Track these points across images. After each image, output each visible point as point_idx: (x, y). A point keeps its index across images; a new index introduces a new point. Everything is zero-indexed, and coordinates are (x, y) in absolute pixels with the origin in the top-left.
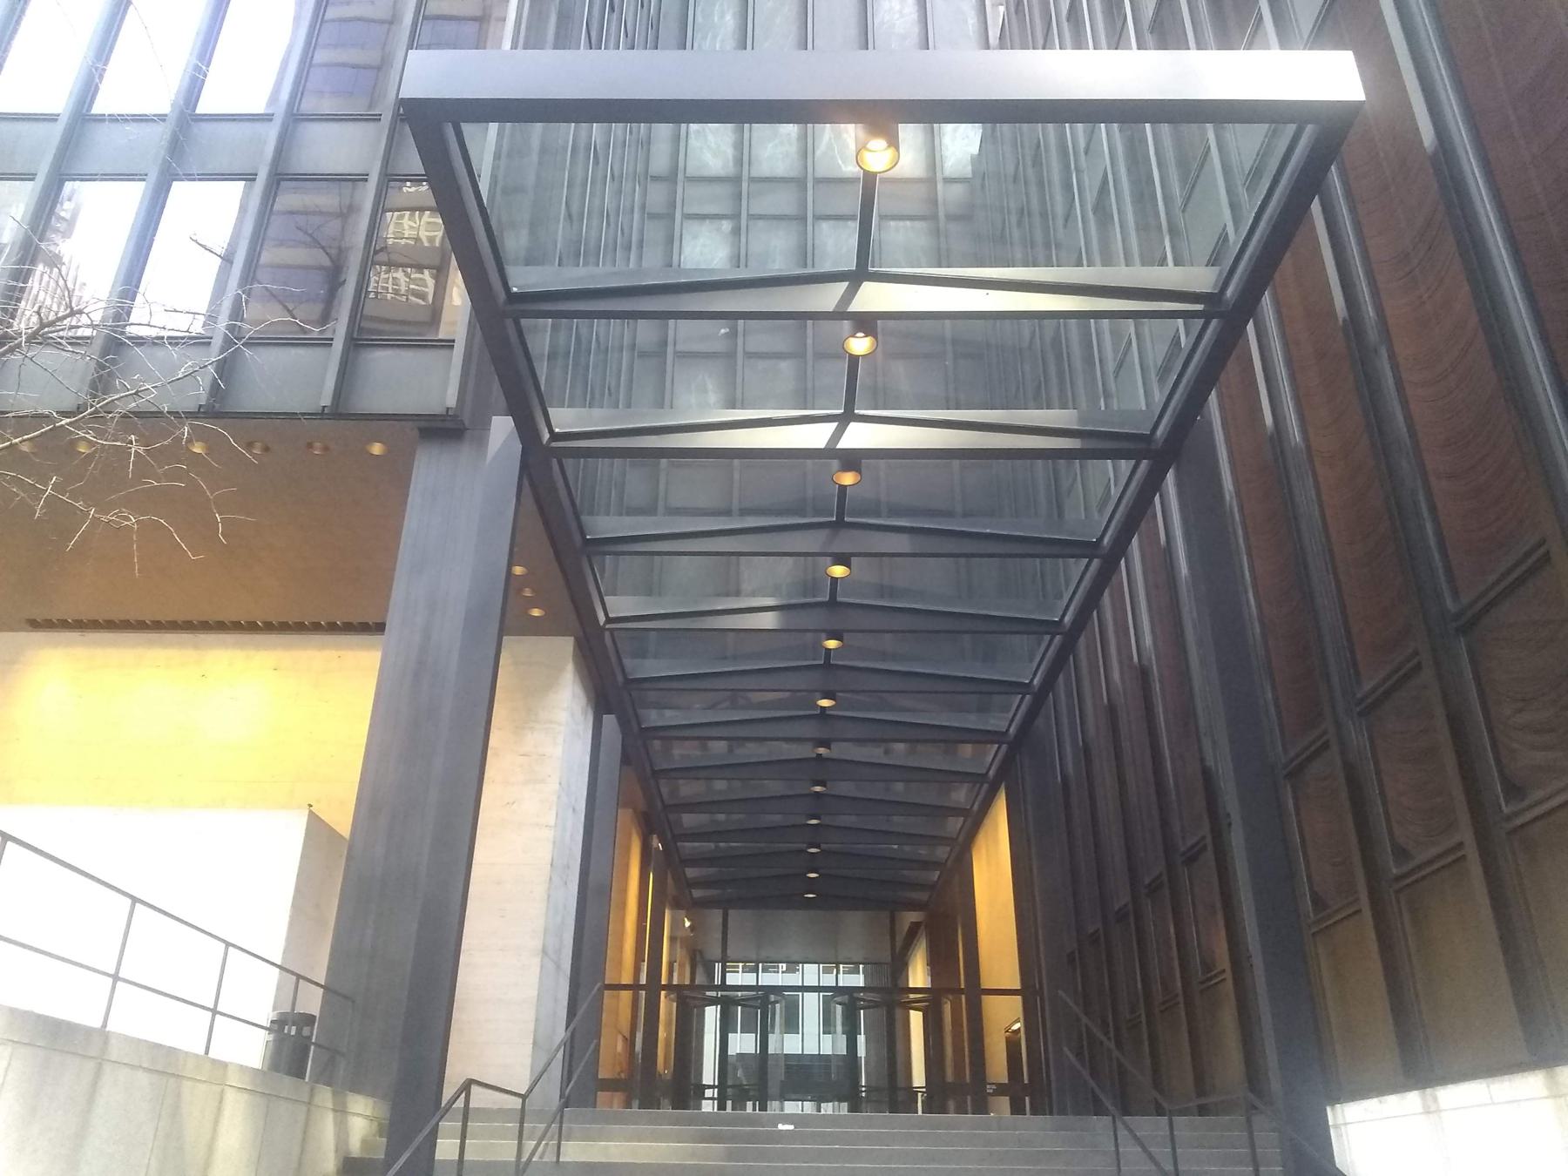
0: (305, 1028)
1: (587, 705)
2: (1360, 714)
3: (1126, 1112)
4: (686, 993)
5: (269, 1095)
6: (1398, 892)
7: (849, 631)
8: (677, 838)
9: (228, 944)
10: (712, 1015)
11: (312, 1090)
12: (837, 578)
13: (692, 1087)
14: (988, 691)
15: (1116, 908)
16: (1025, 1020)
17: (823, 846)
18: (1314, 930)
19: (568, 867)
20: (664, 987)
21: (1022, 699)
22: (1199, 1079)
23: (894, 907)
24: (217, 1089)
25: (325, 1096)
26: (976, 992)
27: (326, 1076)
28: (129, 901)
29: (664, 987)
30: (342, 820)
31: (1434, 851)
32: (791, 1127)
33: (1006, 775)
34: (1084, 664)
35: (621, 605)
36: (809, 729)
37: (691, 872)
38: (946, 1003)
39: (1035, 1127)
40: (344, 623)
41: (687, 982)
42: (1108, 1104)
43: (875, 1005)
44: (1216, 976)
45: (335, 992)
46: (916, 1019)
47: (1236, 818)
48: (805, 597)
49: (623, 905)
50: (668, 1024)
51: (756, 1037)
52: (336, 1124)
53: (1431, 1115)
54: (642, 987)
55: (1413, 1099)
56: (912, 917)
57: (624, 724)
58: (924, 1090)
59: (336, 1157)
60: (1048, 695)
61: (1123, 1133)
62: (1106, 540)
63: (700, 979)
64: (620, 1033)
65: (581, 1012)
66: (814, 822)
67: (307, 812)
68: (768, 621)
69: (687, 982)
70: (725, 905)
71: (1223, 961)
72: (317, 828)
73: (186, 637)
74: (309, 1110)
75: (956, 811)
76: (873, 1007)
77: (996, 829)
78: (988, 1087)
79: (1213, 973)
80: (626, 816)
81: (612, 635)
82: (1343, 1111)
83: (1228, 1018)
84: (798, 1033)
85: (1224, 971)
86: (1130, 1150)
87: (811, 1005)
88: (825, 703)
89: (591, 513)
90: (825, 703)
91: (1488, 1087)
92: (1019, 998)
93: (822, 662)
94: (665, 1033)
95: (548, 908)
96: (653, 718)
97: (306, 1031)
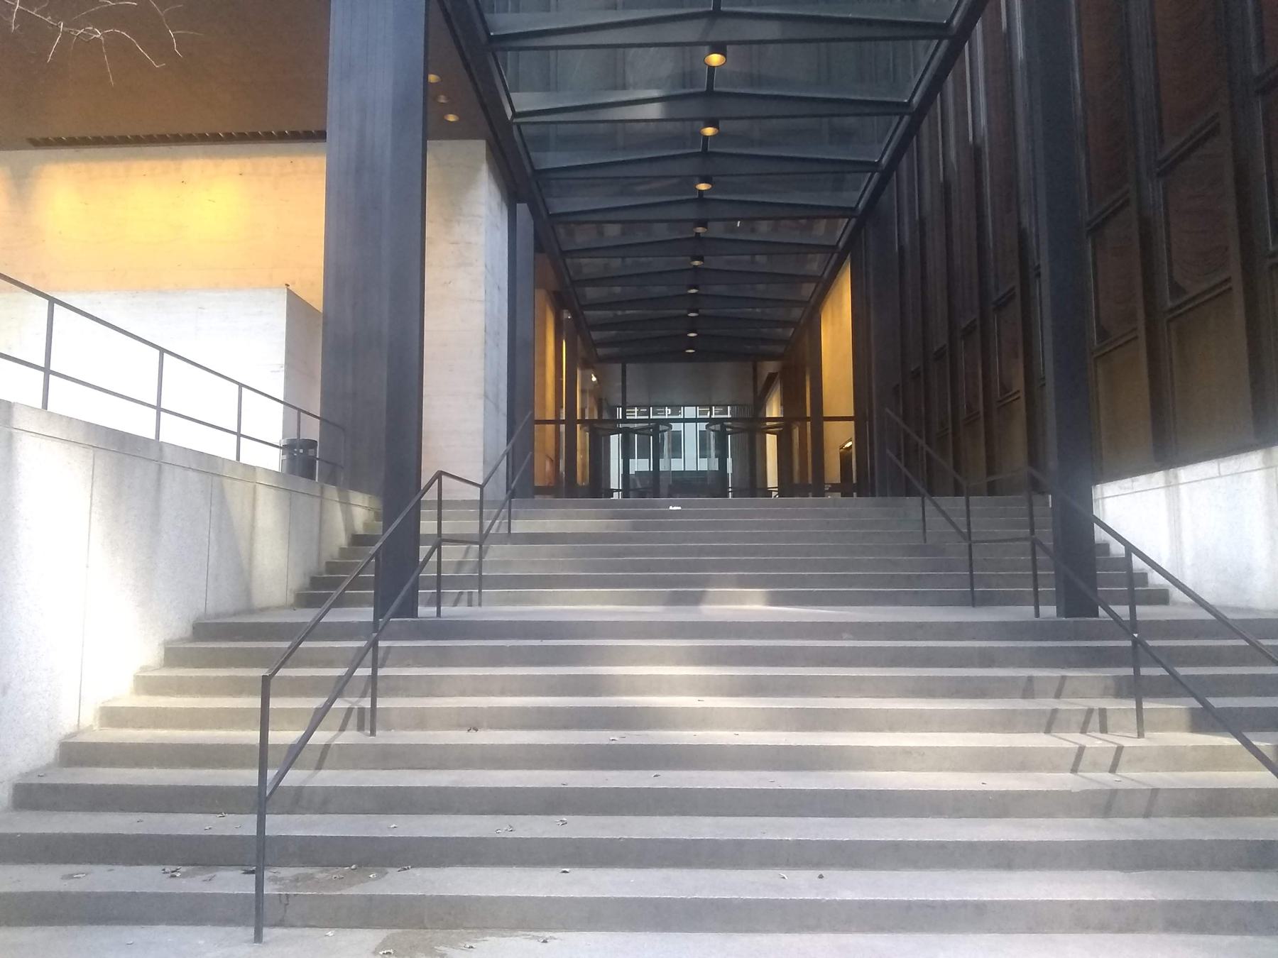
0: (310, 450)
1: (502, 200)
2: (1159, 175)
3: (932, 492)
4: (596, 425)
5: (290, 490)
6: (1170, 321)
8: (583, 307)
9: (241, 385)
10: (615, 440)
11: (322, 488)
12: (714, 67)
13: (603, 491)
14: (840, 171)
15: (935, 350)
16: (856, 439)
17: (700, 311)
18: (1095, 356)
19: (498, 333)
20: (579, 422)
22: (990, 459)
23: (755, 359)
24: (250, 485)
25: (332, 492)
26: (819, 419)
27: (331, 479)
28: (158, 352)
29: (579, 422)
30: (315, 297)
31: (1205, 286)
32: (680, 508)
33: (851, 249)
34: (925, 143)
35: (525, 101)
36: (689, 212)
37: (596, 335)
38: (795, 428)
39: (860, 506)
40: (292, 132)
41: (596, 417)
42: (918, 485)
43: (741, 431)
44: (1011, 396)
45: (327, 421)
46: (771, 441)
47: (1045, 271)
48: (684, 87)
49: (543, 364)
50: (583, 451)
51: (650, 461)
52: (343, 511)
53: (1171, 488)
54: (563, 422)
55: (1158, 477)
56: (770, 367)
57: (534, 211)
58: (777, 489)
59: (346, 534)
61: (929, 507)
62: (955, 22)
63: (606, 416)
64: (548, 457)
65: (517, 432)
66: (693, 291)
67: (286, 291)
68: (653, 111)
69: (596, 417)
70: (623, 360)
71: (1019, 384)
72: (296, 305)
73: (163, 149)
74: (321, 505)
75: (807, 278)
77: (841, 296)
78: (826, 486)
79: (1010, 393)
80: (541, 295)
81: (519, 128)
82: (1102, 489)
83: (1018, 433)
85: (1018, 391)
86: (935, 520)
87: (690, 434)
88: (703, 187)
89: (492, 12)
90: (703, 187)
91: (1219, 465)
92: (852, 423)
93: (700, 150)
94: (582, 457)
95: (485, 364)
96: (560, 205)
97: (311, 452)
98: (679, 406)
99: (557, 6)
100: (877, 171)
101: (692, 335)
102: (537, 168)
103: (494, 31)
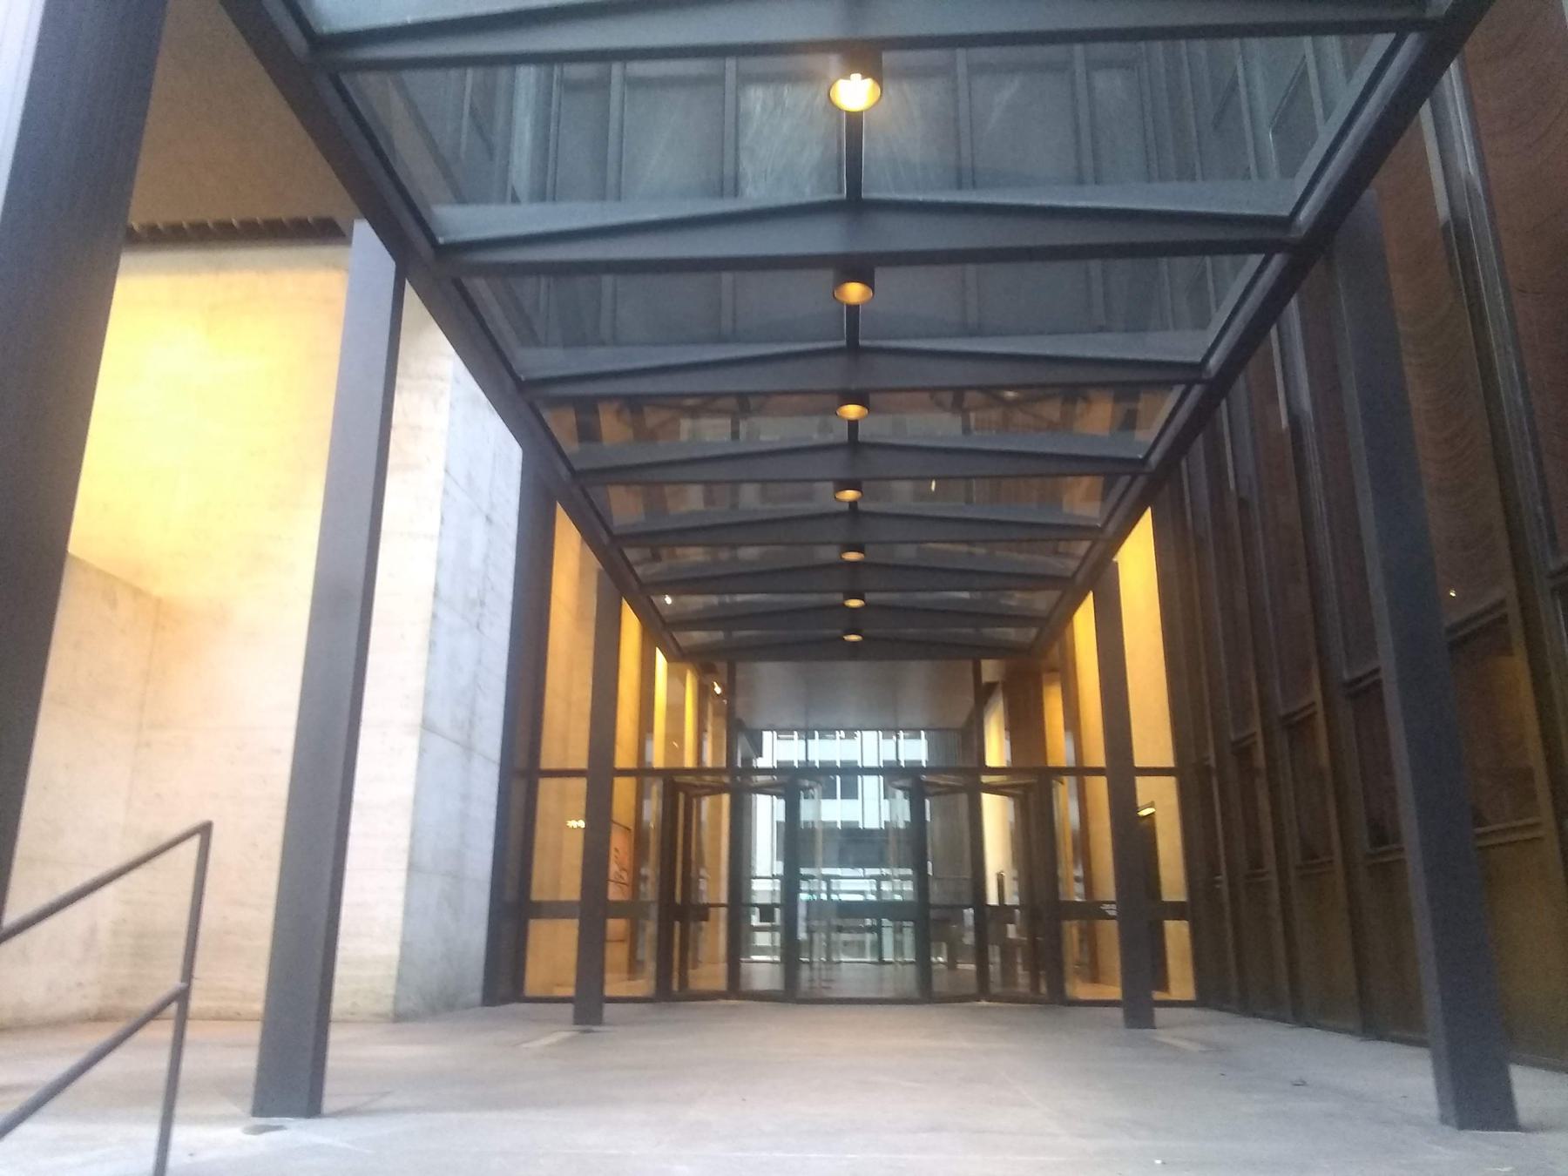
7: (877, 391)
21: (1265, 263)
60: (1218, 405)
62: (1304, 215)
76: (946, 793)
84: (857, 798)
98: (928, 478)
99: (554, 192)
100: (1199, 381)
101: (854, 638)
102: (441, 240)
103: (442, 235)
